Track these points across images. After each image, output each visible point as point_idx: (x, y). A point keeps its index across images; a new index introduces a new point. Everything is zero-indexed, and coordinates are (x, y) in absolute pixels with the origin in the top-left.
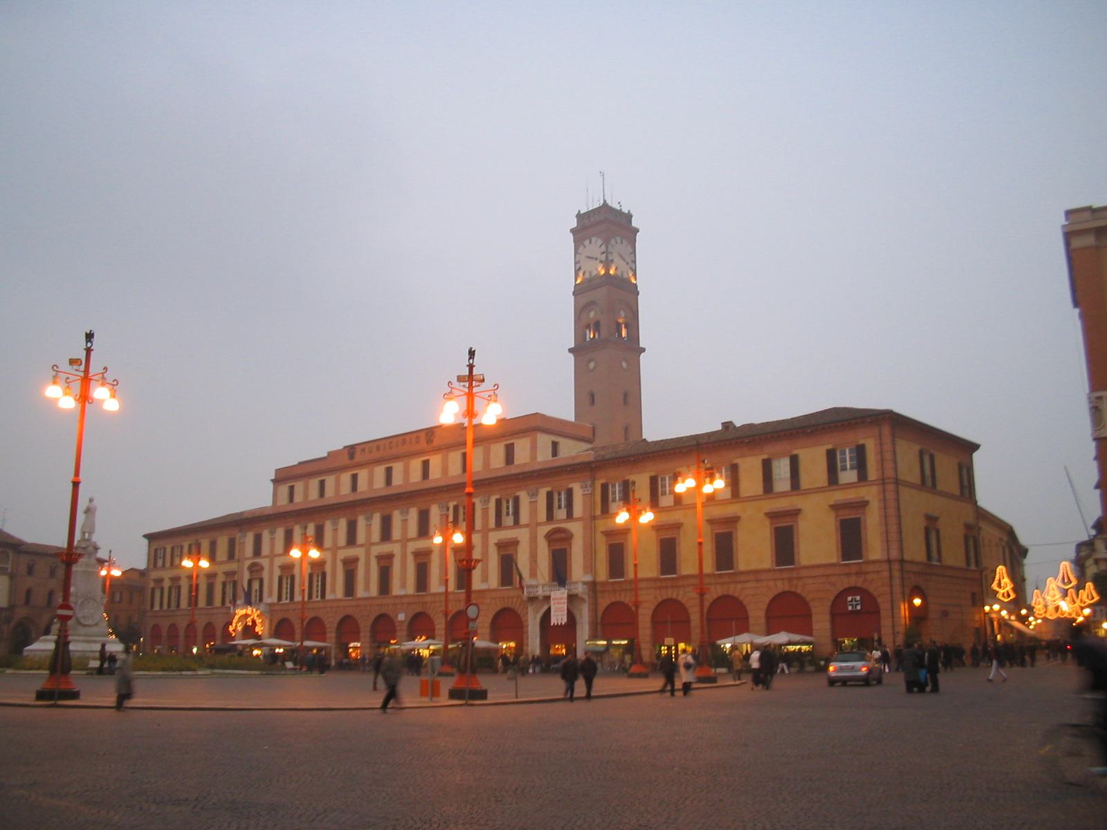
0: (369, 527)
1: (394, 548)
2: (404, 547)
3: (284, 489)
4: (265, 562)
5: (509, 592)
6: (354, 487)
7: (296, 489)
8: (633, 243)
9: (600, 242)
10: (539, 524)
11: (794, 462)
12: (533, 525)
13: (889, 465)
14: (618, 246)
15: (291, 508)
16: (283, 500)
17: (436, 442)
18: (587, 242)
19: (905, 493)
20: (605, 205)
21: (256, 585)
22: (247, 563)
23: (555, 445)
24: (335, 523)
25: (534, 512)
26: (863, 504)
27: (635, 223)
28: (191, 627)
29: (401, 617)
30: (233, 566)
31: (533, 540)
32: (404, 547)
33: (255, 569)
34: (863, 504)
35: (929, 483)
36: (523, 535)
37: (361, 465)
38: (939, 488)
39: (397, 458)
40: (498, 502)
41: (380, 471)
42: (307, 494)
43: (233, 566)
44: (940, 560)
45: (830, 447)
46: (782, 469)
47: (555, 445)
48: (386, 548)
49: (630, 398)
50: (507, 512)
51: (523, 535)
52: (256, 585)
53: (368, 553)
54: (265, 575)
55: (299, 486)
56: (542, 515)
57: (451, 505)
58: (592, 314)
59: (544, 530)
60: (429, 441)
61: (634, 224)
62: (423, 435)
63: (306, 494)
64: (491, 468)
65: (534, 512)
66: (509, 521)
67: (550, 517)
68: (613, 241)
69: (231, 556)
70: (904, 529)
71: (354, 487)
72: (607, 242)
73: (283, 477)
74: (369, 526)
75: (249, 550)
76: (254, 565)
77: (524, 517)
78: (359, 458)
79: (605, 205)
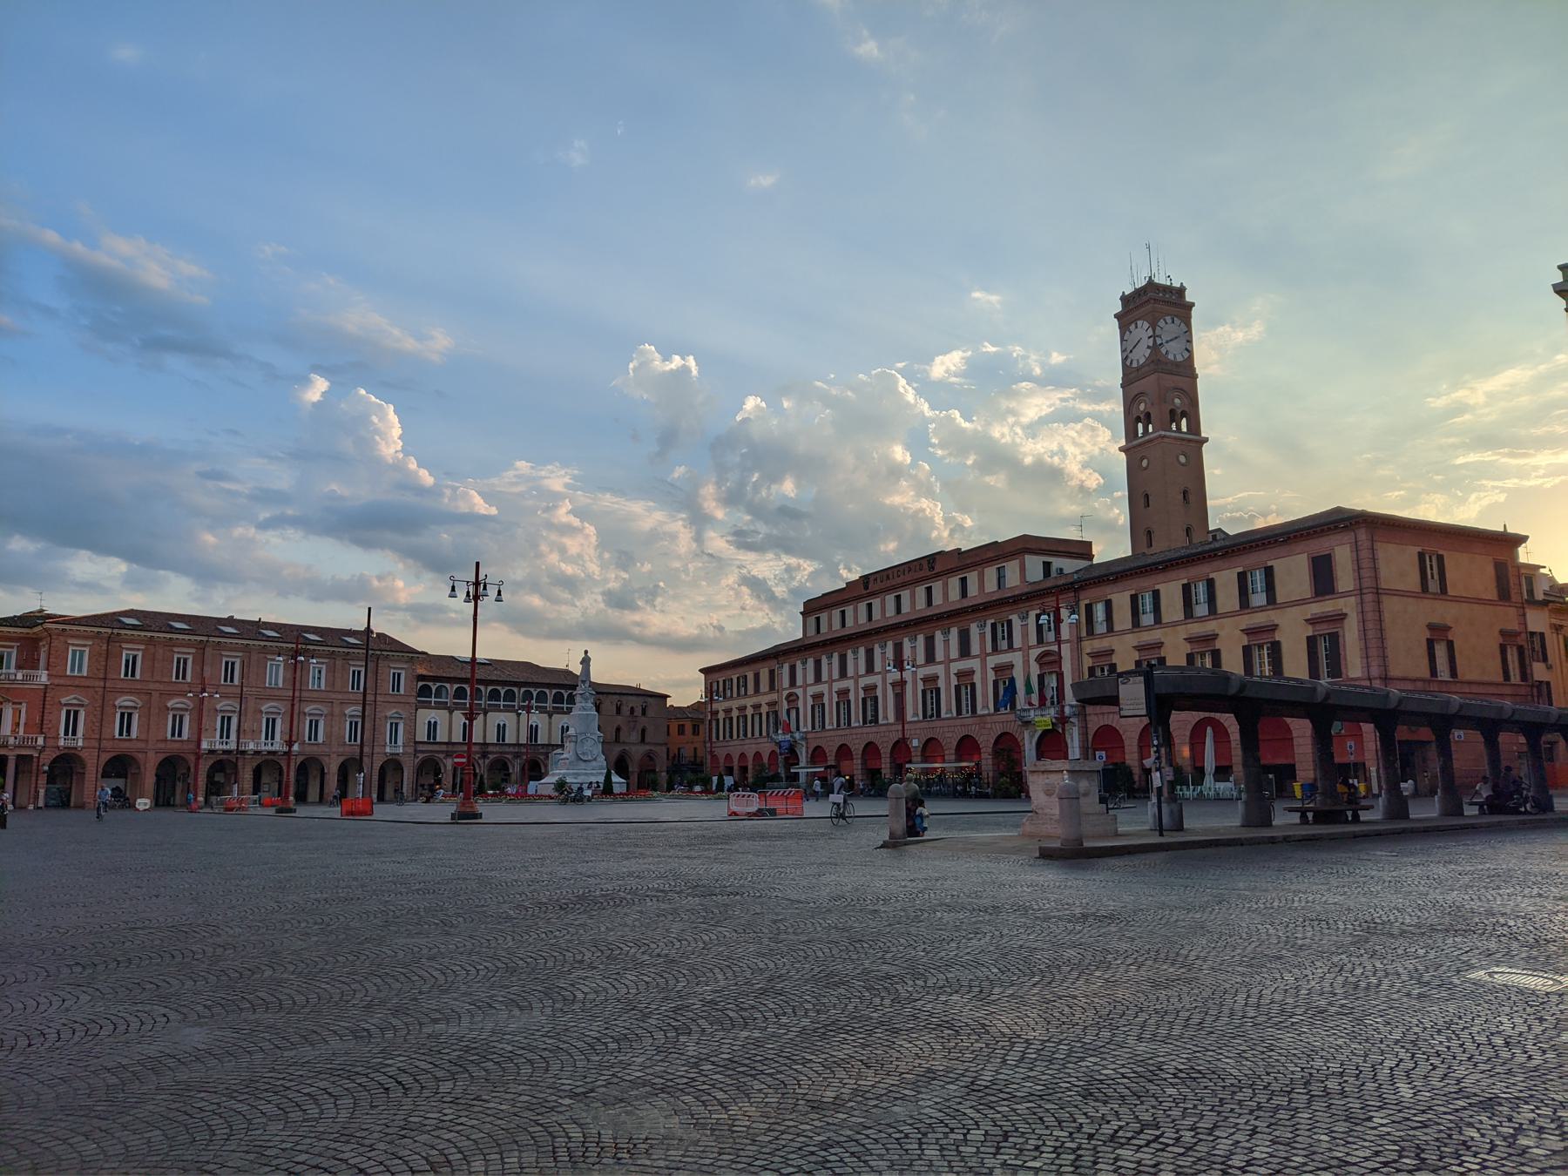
0: (805, 671)
1: (973, 664)
2: (857, 683)
3: (812, 620)
4: (799, 692)
5: (1005, 715)
6: (964, 593)
7: (903, 601)
8: (1187, 321)
9: (1146, 325)
10: (1030, 648)
11: (1108, 604)
12: (1026, 649)
13: (1366, 573)
14: (1168, 328)
15: (966, 603)
16: (812, 631)
17: (938, 569)
18: (1132, 327)
19: (1391, 605)
20: (1151, 283)
21: (1052, 682)
22: (785, 693)
23: (1047, 565)
24: (855, 652)
25: (1025, 635)
26: (1340, 617)
27: (1189, 298)
28: (901, 747)
29: (915, 743)
30: (774, 697)
31: (1026, 663)
32: (857, 683)
33: (792, 699)
34: (1340, 617)
35: (1433, 586)
36: (1016, 658)
37: (873, 594)
38: (1450, 592)
39: (904, 586)
40: (994, 626)
41: (954, 582)
42: (831, 623)
43: (774, 697)
44: (1453, 673)
45: (1240, 569)
46: (1099, 612)
47: (1047, 565)
48: (870, 680)
49: (1194, 494)
50: (1002, 637)
51: (1016, 658)
52: (1052, 682)
53: (884, 680)
54: (800, 704)
55: (824, 617)
56: (1033, 639)
57: (989, 622)
58: (1142, 407)
59: (1035, 653)
60: (866, 588)
61: (1188, 299)
62: (925, 563)
63: (946, 595)
64: (1095, 561)
65: (1025, 635)
66: (1004, 645)
67: (1040, 640)
68: (1161, 323)
69: (772, 688)
70: (1389, 643)
71: (964, 593)
72: (1153, 325)
73: (813, 608)
74: (947, 642)
75: (786, 683)
76: (790, 695)
77: (1017, 643)
78: (872, 587)
79: (1151, 283)
